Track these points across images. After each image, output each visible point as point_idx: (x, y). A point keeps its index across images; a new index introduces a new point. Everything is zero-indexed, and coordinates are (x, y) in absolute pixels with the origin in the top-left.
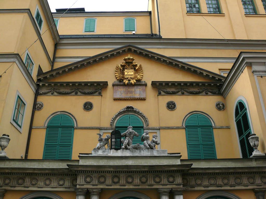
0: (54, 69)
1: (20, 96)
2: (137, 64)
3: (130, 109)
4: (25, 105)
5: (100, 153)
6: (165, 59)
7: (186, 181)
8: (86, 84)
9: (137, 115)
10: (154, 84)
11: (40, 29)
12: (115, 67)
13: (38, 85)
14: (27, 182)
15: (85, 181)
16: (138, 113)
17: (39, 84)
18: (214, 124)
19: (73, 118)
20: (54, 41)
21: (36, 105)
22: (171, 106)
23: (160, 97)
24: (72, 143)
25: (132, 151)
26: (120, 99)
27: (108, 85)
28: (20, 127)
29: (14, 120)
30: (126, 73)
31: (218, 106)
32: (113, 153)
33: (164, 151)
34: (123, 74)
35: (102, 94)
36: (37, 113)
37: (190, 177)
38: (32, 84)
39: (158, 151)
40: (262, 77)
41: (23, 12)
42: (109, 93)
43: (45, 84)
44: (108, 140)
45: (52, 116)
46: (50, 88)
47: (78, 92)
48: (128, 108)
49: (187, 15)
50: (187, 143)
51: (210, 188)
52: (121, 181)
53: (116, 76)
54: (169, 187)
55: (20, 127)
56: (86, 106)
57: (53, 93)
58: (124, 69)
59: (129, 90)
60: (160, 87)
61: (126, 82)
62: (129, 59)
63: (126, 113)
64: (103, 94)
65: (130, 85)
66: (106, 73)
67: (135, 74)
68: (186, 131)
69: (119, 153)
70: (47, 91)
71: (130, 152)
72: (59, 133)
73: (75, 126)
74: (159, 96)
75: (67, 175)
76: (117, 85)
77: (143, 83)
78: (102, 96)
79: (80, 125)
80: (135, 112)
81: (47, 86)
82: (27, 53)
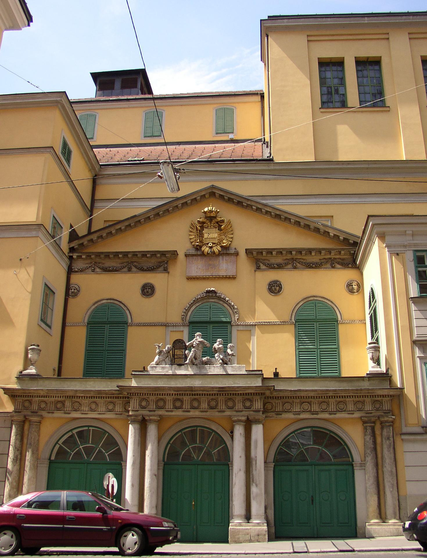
0: (93, 230)
1: (48, 284)
2: (222, 219)
4: (54, 293)
6: (268, 210)
7: (271, 406)
9: (221, 302)
10: (248, 252)
11: (69, 166)
12: (189, 224)
13: (71, 258)
14: (367, 415)
15: (140, 405)
17: (72, 256)
18: (341, 317)
19: (125, 308)
20: (91, 172)
21: (69, 289)
22: (275, 288)
23: (259, 274)
24: (126, 348)
25: (200, 367)
26: (197, 278)
27: (178, 254)
28: (50, 327)
29: (42, 320)
30: (206, 236)
31: (350, 287)
34: (201, 235)
35: (169, 270)
37: (277, 401)
38: (63, 259)
40: (398, 254)
41: (43, 152)
42: (179, 268)
43: (81, 256)
44: (169, 352)
45: (94, 307)
46: (89, 261)
47: (133, 267)
48: (208, 292)
51: (302, 416)
52: (184, 406)
53: (191, 239)
55: (50, 327)
56: (145, 290)
57: (94, 269)
58: (202, 228)
59: (211, 262)
60: (260, 258)
61: (206, 249)
62: (211, 211)
63: (205, 301)
64: (170, 270)
66: (172, 235)
67: (220, 235)
68: (295, 327)
69: (181, 371)
70: (85, 266)
71: (197, 369)
72: (105, 341)
73: (130, 321)
74: (257, 272)
76: (193, 255)
77: (232, 251)
78: (169, 273)
79: (136, 320)
80: (219, 298)
81: (84, 259)
82: (52, 216)
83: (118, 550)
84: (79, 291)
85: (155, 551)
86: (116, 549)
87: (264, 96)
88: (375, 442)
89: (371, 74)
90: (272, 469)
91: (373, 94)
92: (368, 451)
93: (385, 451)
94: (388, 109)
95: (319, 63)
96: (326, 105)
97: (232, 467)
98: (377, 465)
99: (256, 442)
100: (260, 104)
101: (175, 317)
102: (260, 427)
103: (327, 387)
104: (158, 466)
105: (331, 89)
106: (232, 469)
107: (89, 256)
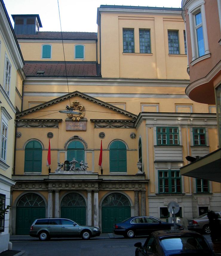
3: (76, 138)
5: (59, 172)
8: (48, 121)
9: (80, 141)
15: (53, 186)
16: (81, 140)
22: (102, 135)
23: (96, 129)
32: (65, 172)
33: (90, 172)
36: (18, 139)
39: (87, 171)
40: (150, 128)
47: (44, 125)
48: (75, 136)
49: (123, 55)
50: (110, 159)
54: (92, 189)
59: (76, 124)
60: (95, 122)
64: (59, 127)
65: (76, 121)
69: (68, 173)
73: (43, 148)
75: (43, 183)
77: (85, 120)
78: (58, 128)
80: (79, 139)
83: (39, 239)
84: (21, 135)
85: (147, 238)
86: (81, 238)
87: (97, 41)
88: (138, 199)
89: (146, 36)
90: (101, 210)
91: (146, 46)
92: (136, 202)
93: (142, 202)
94: (152, 54)
95: (123, 30)
96: (125, 51)
97: (87, 208)
98: (139, 207)
99: (96, 199)
100: (96, 44)
101: (62, 147)
102: (97, 193)
103: (121, 179)
104: (60, 208)
105: (128, 43)
106: (87, 209)
107: (24, 120)
